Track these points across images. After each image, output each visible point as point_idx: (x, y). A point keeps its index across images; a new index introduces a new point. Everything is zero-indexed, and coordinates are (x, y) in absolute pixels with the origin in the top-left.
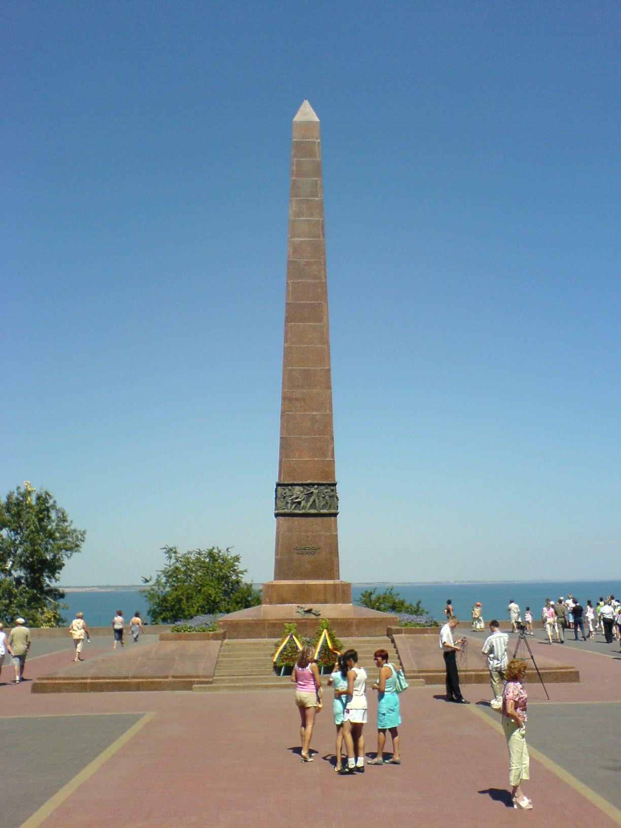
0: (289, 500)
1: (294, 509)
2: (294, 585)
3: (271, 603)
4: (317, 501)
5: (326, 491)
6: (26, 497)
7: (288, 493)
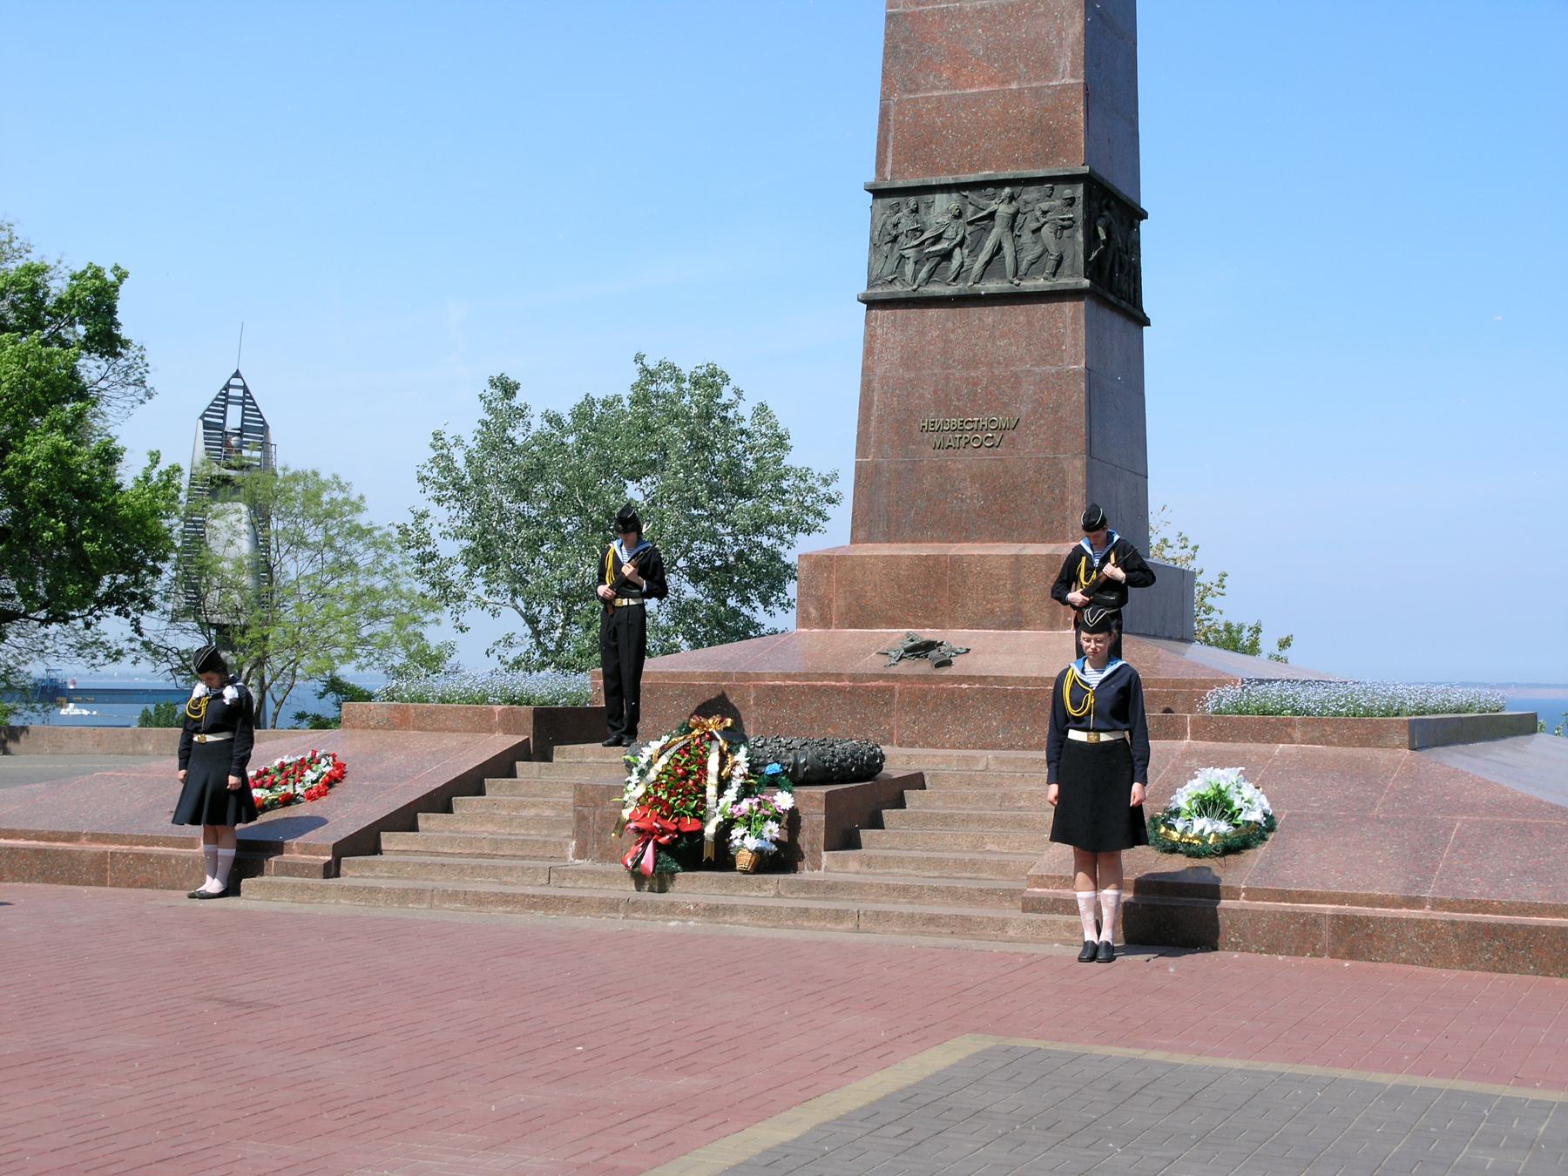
1: (928, 281)
2: (909, 557)
5: (1044, 206)
6: (979, 538)
7: (907, 224)
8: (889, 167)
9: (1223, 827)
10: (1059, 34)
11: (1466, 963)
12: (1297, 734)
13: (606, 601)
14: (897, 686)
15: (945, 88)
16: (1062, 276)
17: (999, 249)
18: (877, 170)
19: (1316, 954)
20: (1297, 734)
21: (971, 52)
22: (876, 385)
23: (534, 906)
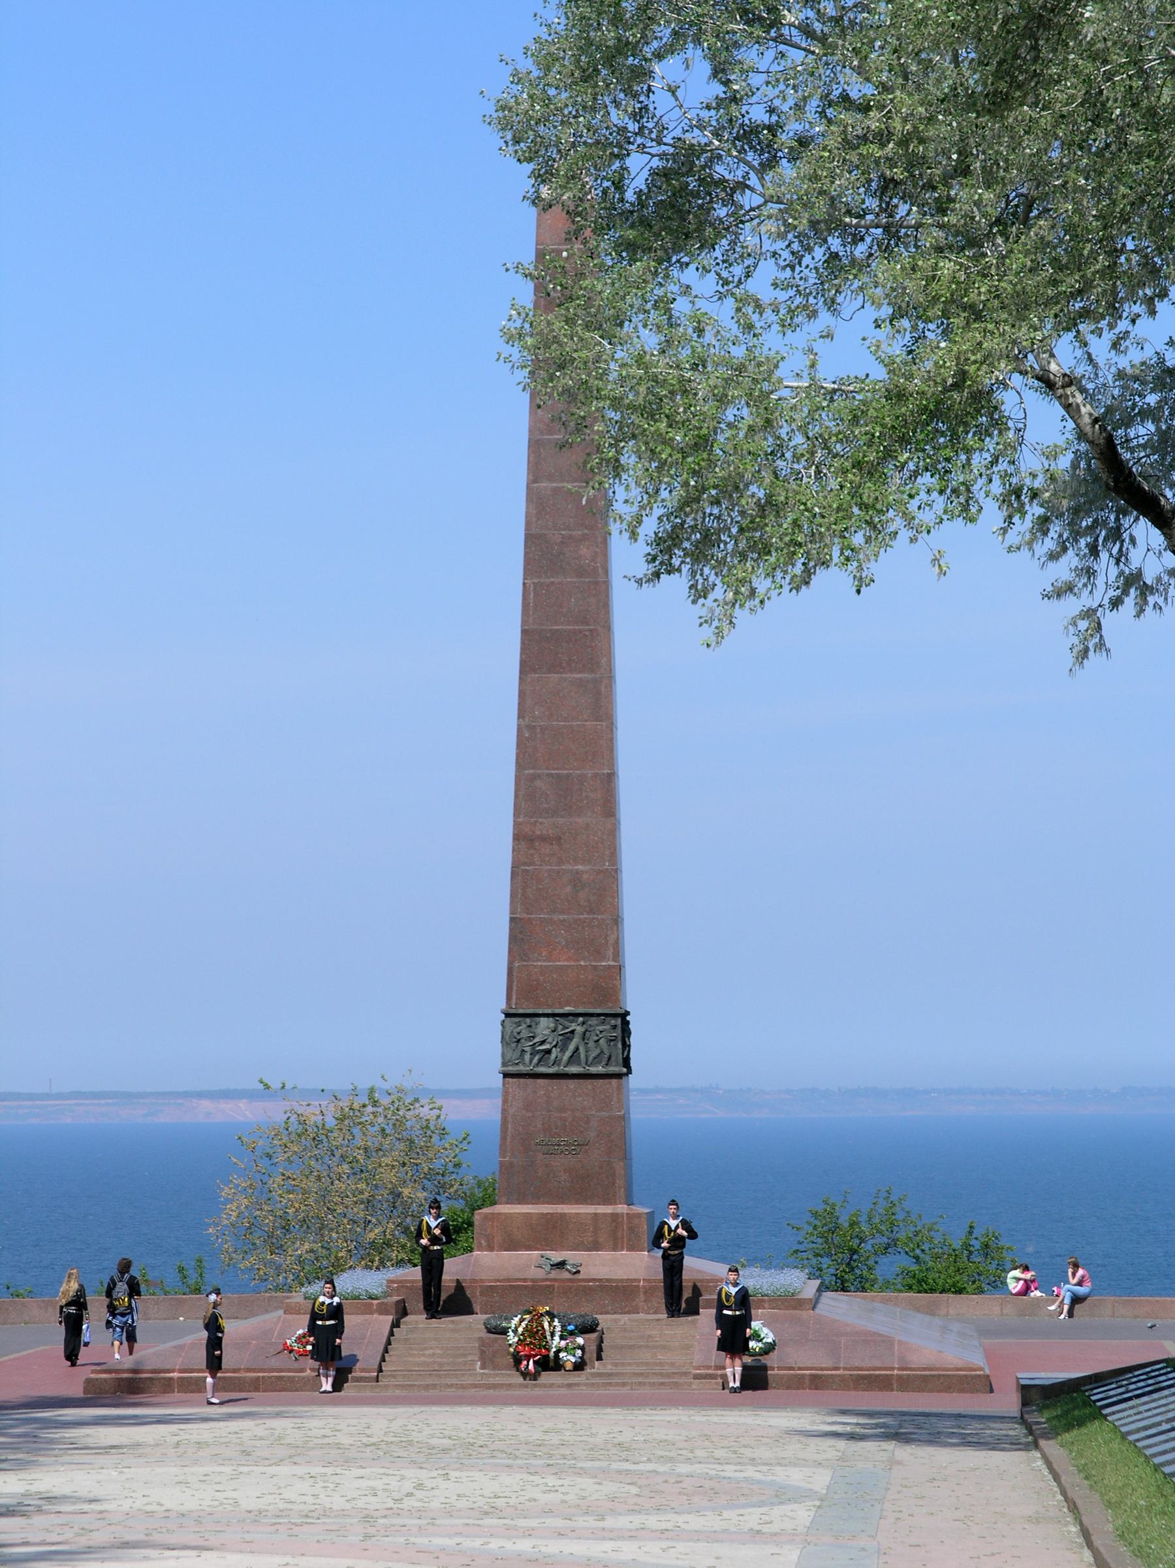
0: (527, 1046)
1: (537, 1065)
3: (490, 1248)
4: (582, 1050)
5: (601, 1028)
7: (525, 1034)
8: (514, 1001)
9: (760, 1345)
10: (605, 938)
11: (856, 1389)
12: (766, 1305)
13: (425, 1248)
14: (556, 1284)
15: (544, 961)
16: (611, 1066)
17: (577, 1049)
18: (507, 1003)
19: (804, 1389)
20: (766, 1305)
21: (558, 943)
22: (510, 1119)
23: (489, 1388)
